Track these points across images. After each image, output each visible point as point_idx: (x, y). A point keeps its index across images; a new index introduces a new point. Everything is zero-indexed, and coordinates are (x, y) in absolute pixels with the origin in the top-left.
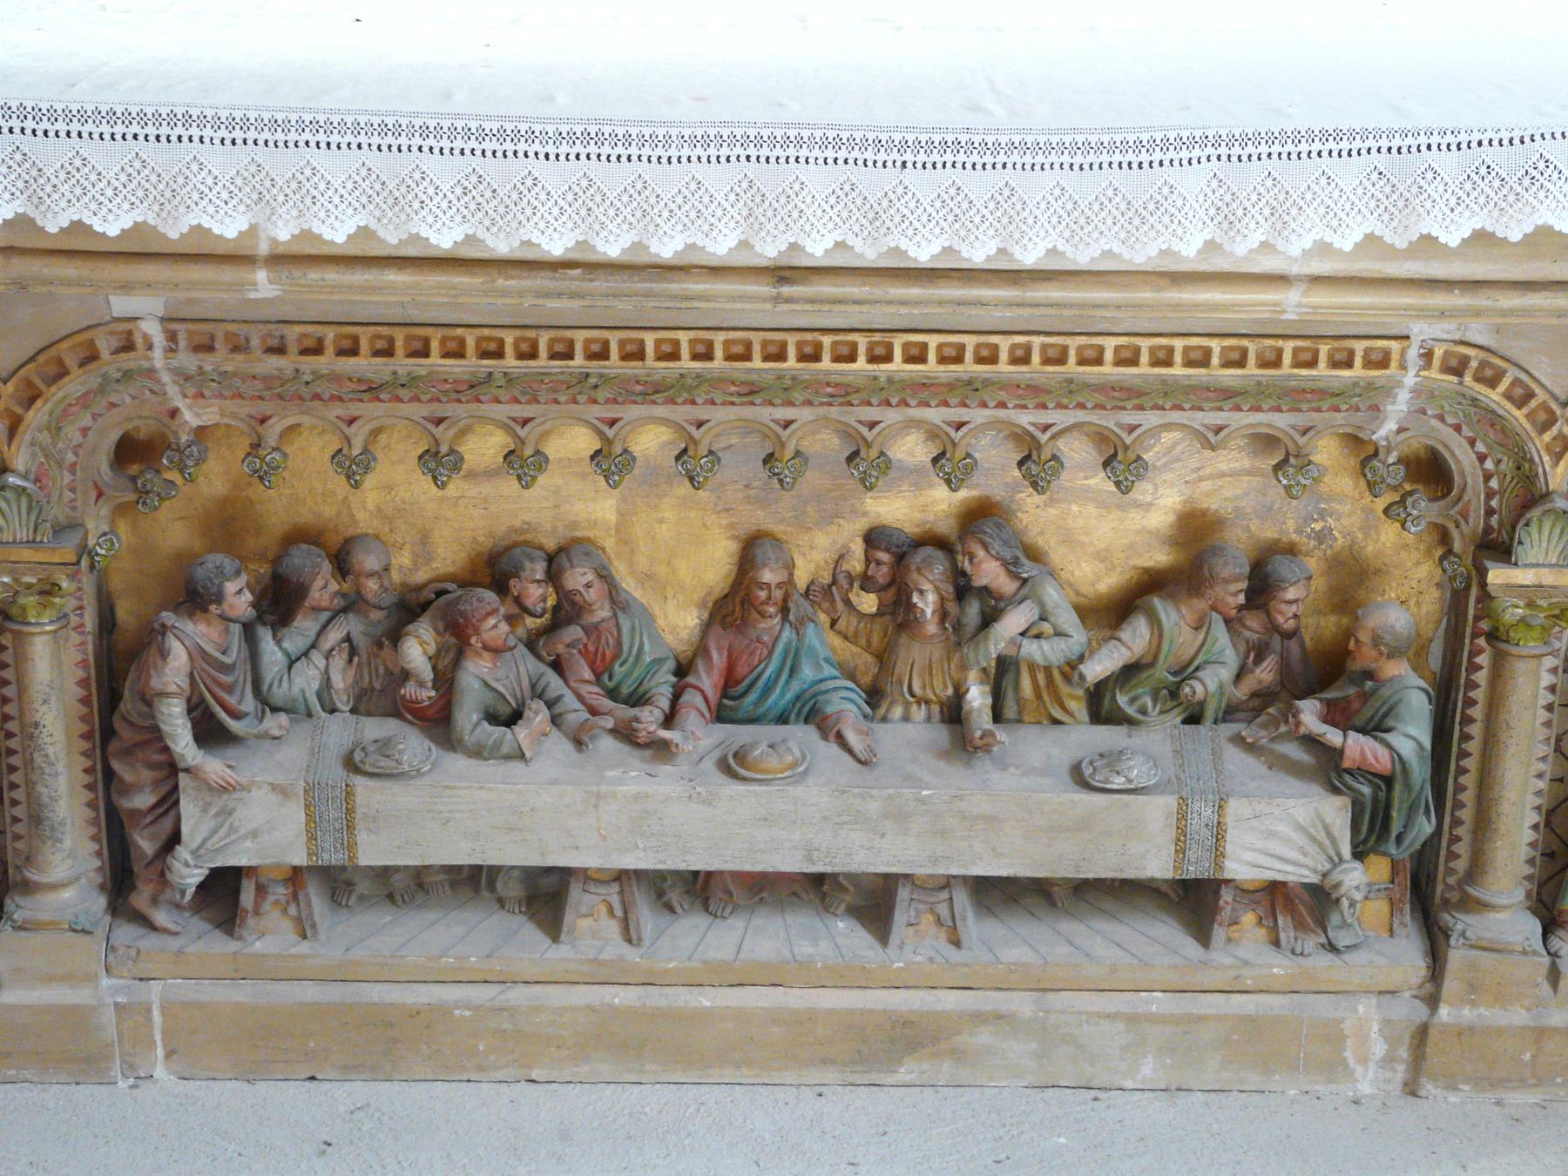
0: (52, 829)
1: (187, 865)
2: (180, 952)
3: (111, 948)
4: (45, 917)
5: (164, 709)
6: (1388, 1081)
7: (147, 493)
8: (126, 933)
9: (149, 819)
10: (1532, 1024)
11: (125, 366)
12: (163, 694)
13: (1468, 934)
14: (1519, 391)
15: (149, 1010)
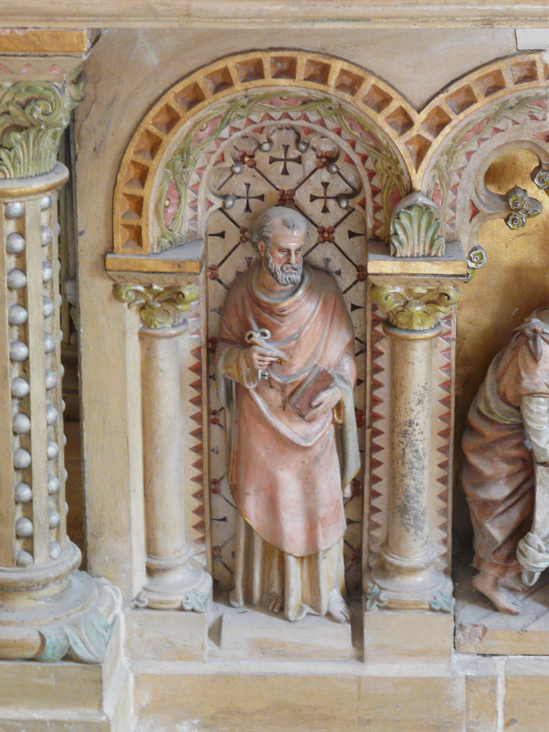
0: (416, 517)
1: (540, 551)
2: (524, 630)
3: (458, 628)
4: (408, 598)
5: (534, 407)
7: (517, 210)
8: (471, 614)
9: (501, 509)
11: (524, 94)
12: (532, 394)
15: (494, 683)
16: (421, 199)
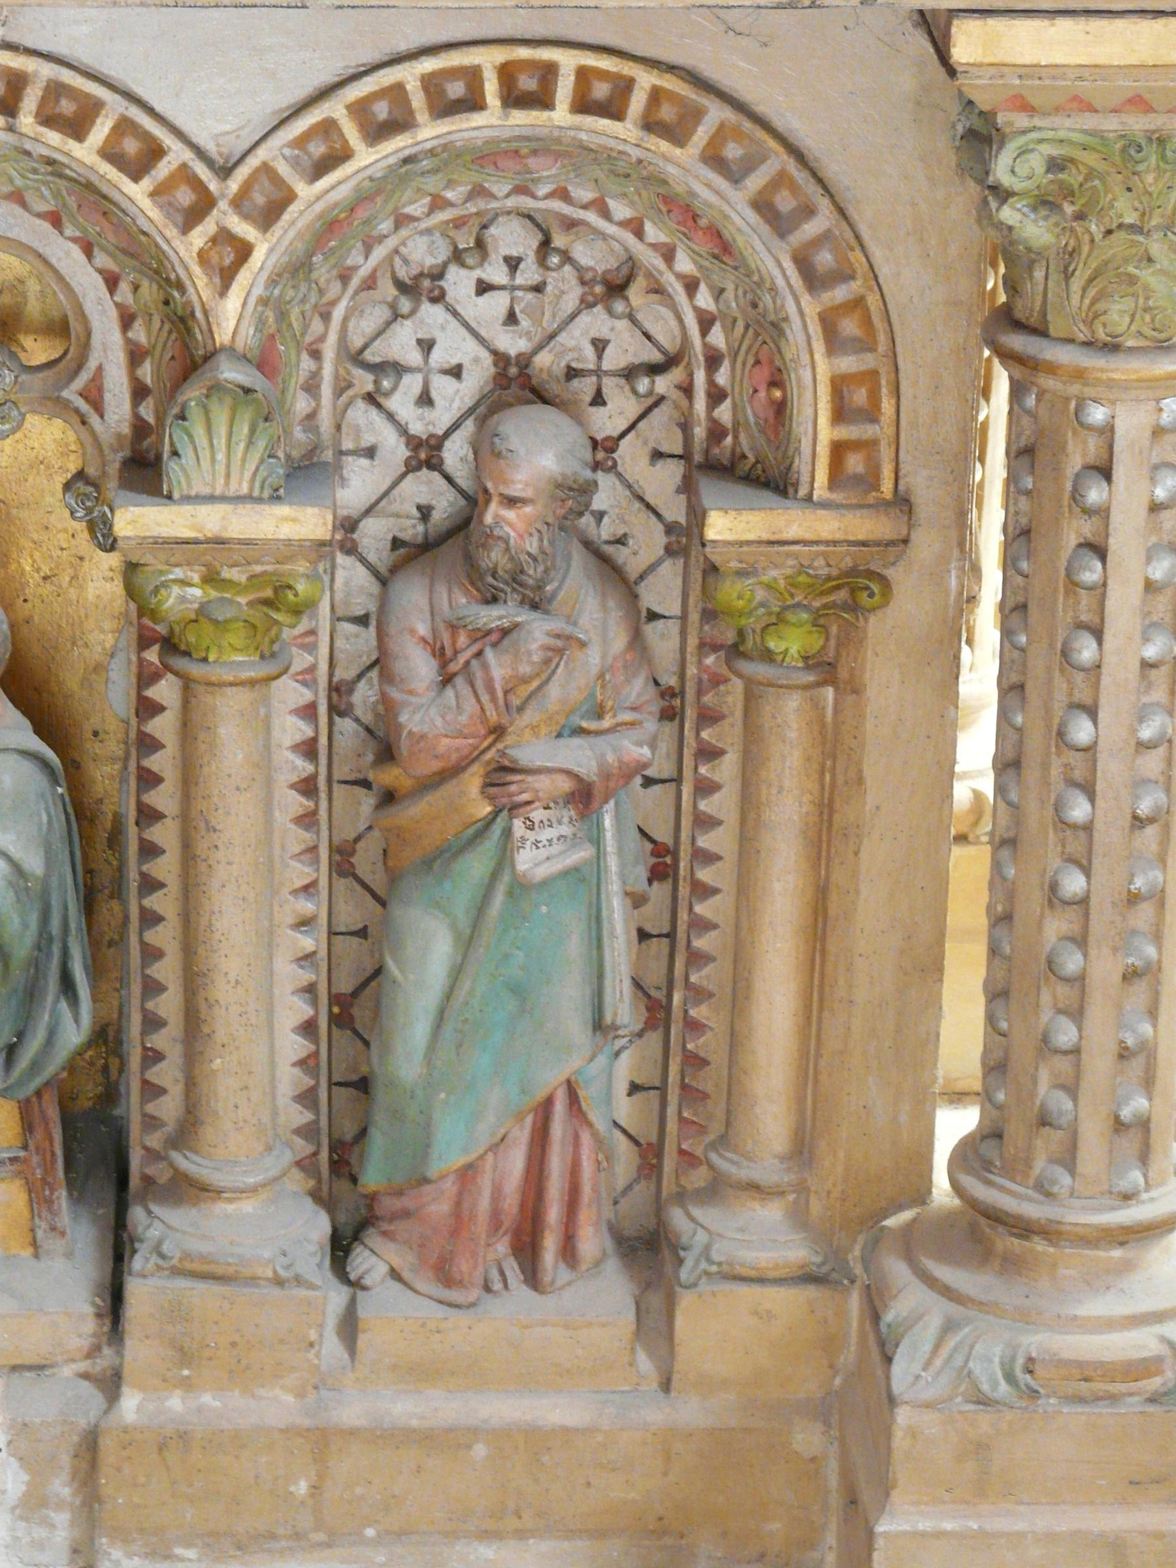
6: (39, 1545)
10: (307, 1422)
13: (165, 1248)
14: (131, 146)
16: (231, 373)
